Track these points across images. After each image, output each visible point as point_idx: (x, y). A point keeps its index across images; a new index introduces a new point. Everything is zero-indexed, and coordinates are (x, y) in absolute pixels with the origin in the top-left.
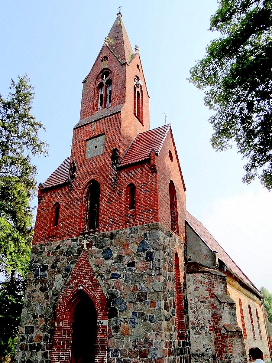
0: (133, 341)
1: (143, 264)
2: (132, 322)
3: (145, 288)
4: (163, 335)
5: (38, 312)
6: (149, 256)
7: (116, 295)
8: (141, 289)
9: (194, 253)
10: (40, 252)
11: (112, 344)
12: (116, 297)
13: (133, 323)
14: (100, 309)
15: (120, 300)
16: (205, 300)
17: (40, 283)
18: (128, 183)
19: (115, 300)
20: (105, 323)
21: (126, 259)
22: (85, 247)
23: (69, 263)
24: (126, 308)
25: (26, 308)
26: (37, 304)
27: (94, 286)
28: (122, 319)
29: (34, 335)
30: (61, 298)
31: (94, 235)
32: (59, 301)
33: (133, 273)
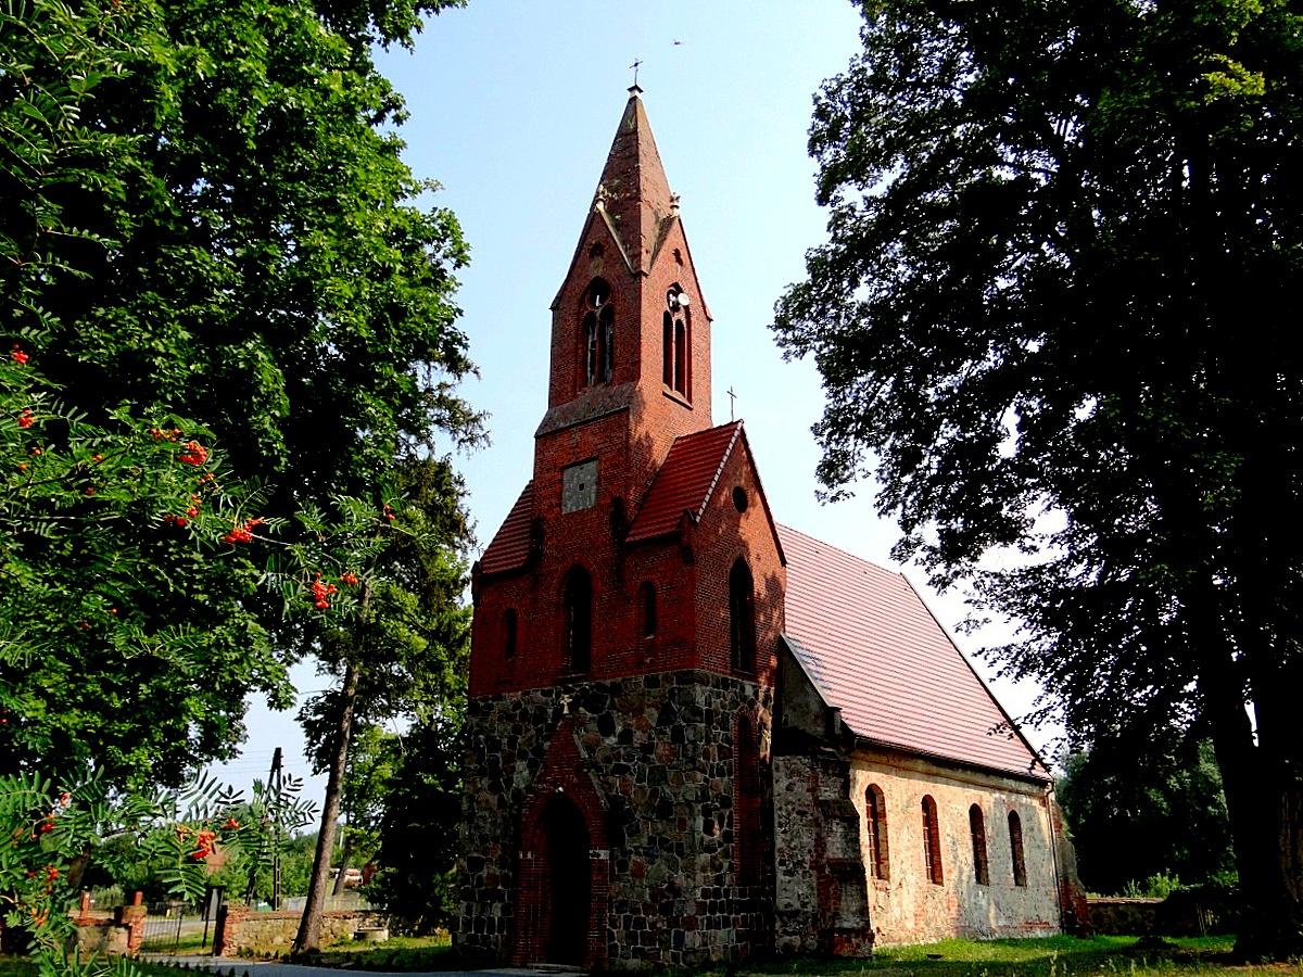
4: (697, 877)
6: (678, 735)
9: (794, 710)
16: (805, 809)
20: (604, 855)
29: (484, 873)
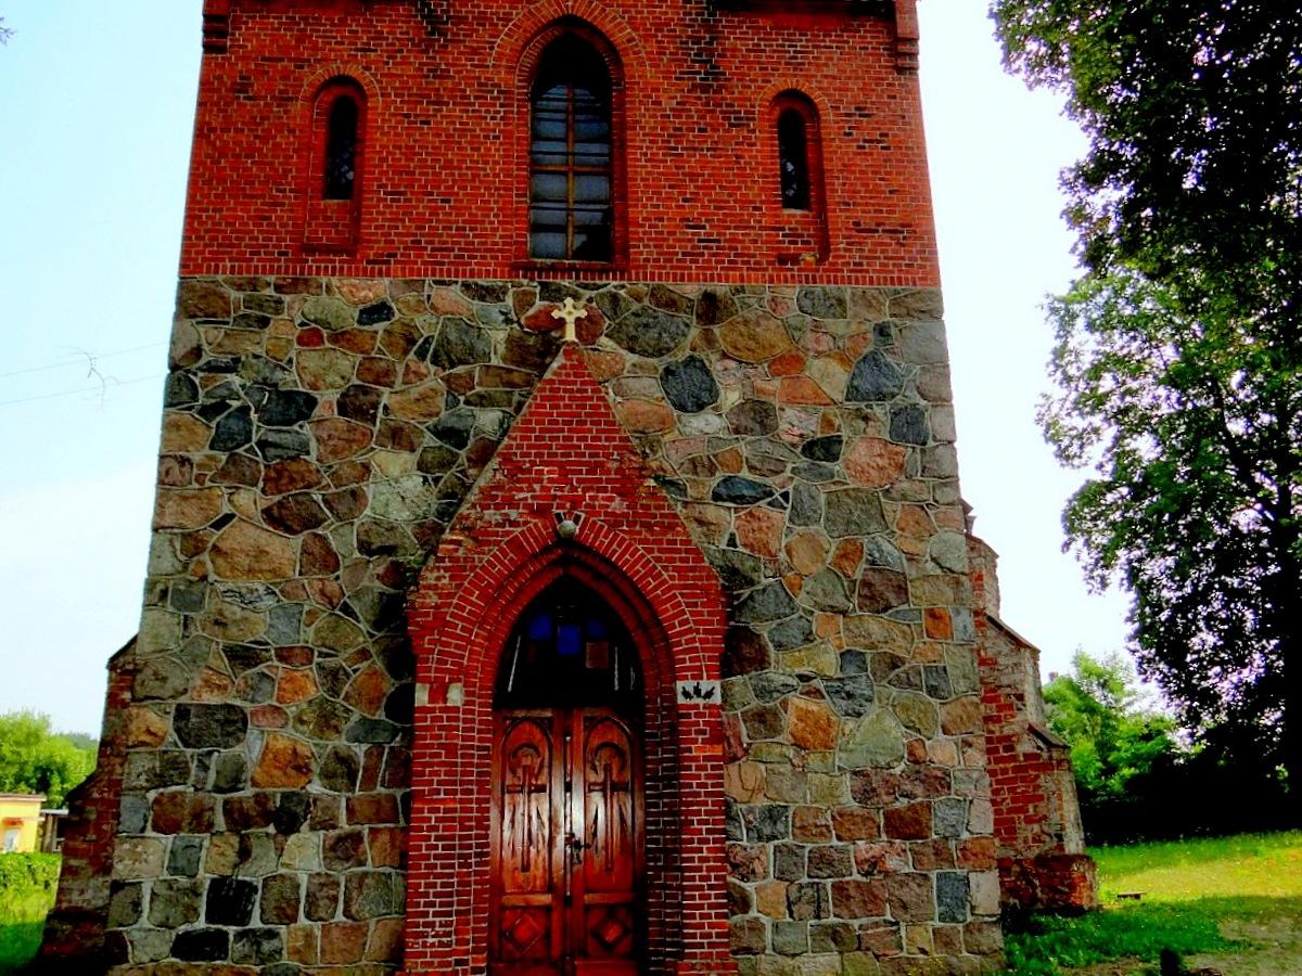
0: (855, 773)
1: (881, 456)
2: (843, 695)
3: (896, 553)
5: (263, 625)
7: (755, 576)
8: (877, 555)
10: (244, 316)
11: (750, 784)
12: (751, 583)
13: (850, 696)
14: (690, 631)
15: (777, 596)
17: (261, 484)
18: (780, 83)
19: (751, 597)
21: (796, 423)
22: (570, 334)
23: (462, 398)
24: (811, 633)
25: (171, 609)
26: (251, 591)
27: (649, 527)
28: (794, 682)
30: (446, 569)
31: (605, 285)
32: (433, 582)
33: (833, 488)
